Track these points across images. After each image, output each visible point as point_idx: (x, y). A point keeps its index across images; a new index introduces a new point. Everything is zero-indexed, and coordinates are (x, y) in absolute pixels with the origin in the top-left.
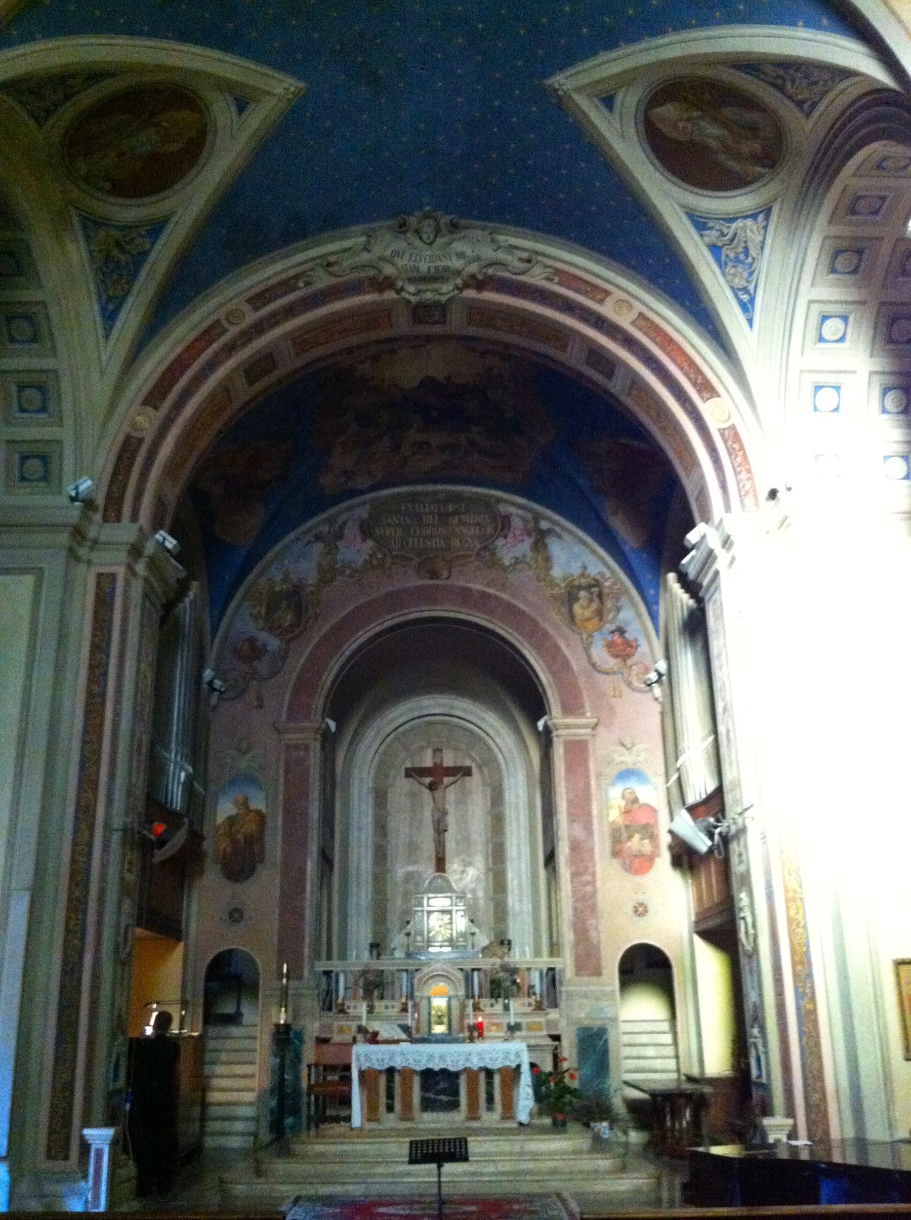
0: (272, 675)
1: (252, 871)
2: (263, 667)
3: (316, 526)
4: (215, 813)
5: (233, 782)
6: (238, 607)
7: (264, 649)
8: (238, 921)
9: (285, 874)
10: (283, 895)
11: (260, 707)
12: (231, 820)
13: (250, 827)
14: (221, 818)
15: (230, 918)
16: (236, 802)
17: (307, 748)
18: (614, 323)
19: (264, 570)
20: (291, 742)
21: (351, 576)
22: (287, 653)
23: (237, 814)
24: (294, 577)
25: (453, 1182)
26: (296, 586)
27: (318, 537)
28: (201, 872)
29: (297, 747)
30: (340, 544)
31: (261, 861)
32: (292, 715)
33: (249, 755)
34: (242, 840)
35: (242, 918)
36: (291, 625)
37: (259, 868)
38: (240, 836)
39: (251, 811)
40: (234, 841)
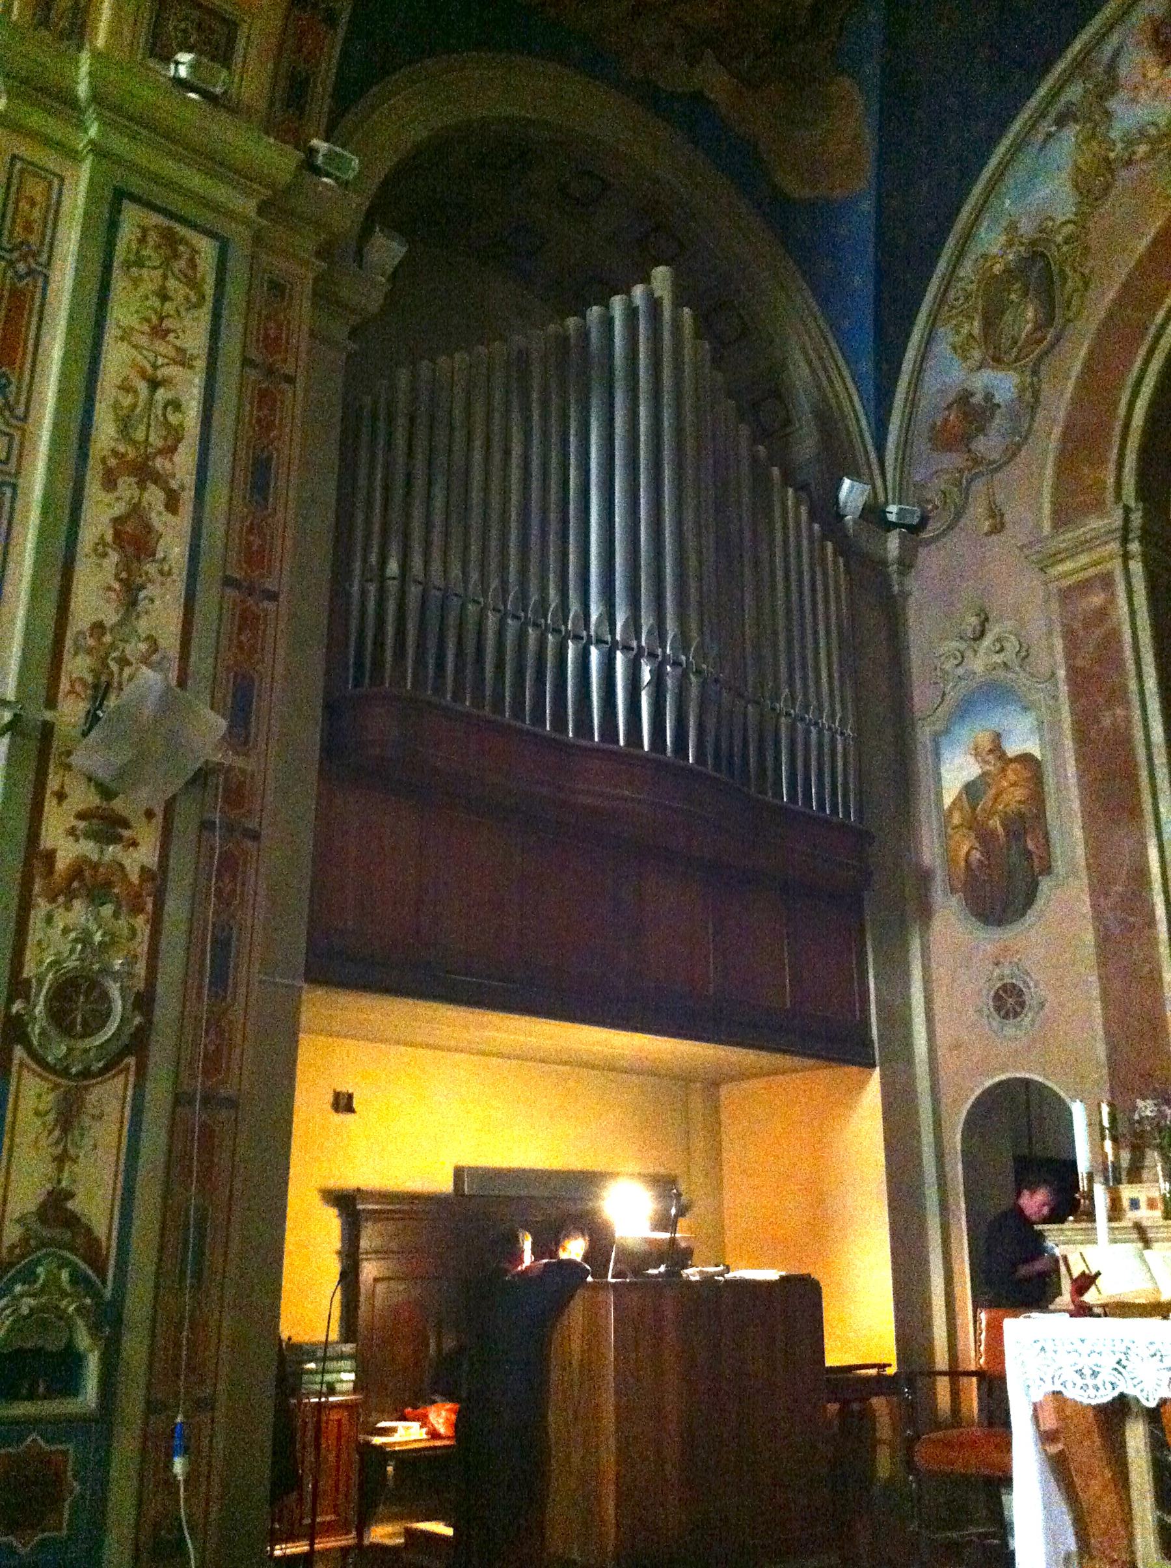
0: (1012, 453)
1: (1030, 898)
2: (988, 445)
3: (1055, 94)
4: (938, 778)
5: (965, 709)
6: (929, 340)
7: (991, 404)
8: (1016, 1014)
9: (1099, 887)
10: (1104, 940)
11: (998, 528)
12: (971, 790)
13: (1015, 797)
14: (950, 792)
15: (998, 1009)
16: (977, 753)
17: (1106, 581)
18: (494, 1170)
19: (968, 236)
20: (1065, 583)
21: (1153, 153)
22: (1036, 394)
23: (984, 774)
24: (1026, 228)
25: (700, 604)
26: (1033, 243)
27: (1061, 121)
28: (925, 912)
29: (1084, 587)
30: (1112, 104)
31: (1047, 870)
32: (1062, 518)
33: (987, 642)
34: (1000, 830)
35: (1022, 1005)
36: (1037, 328)
37: (1045, 884)
38: (995, 823)
39: (1011, 760)
40: (985, 838)
